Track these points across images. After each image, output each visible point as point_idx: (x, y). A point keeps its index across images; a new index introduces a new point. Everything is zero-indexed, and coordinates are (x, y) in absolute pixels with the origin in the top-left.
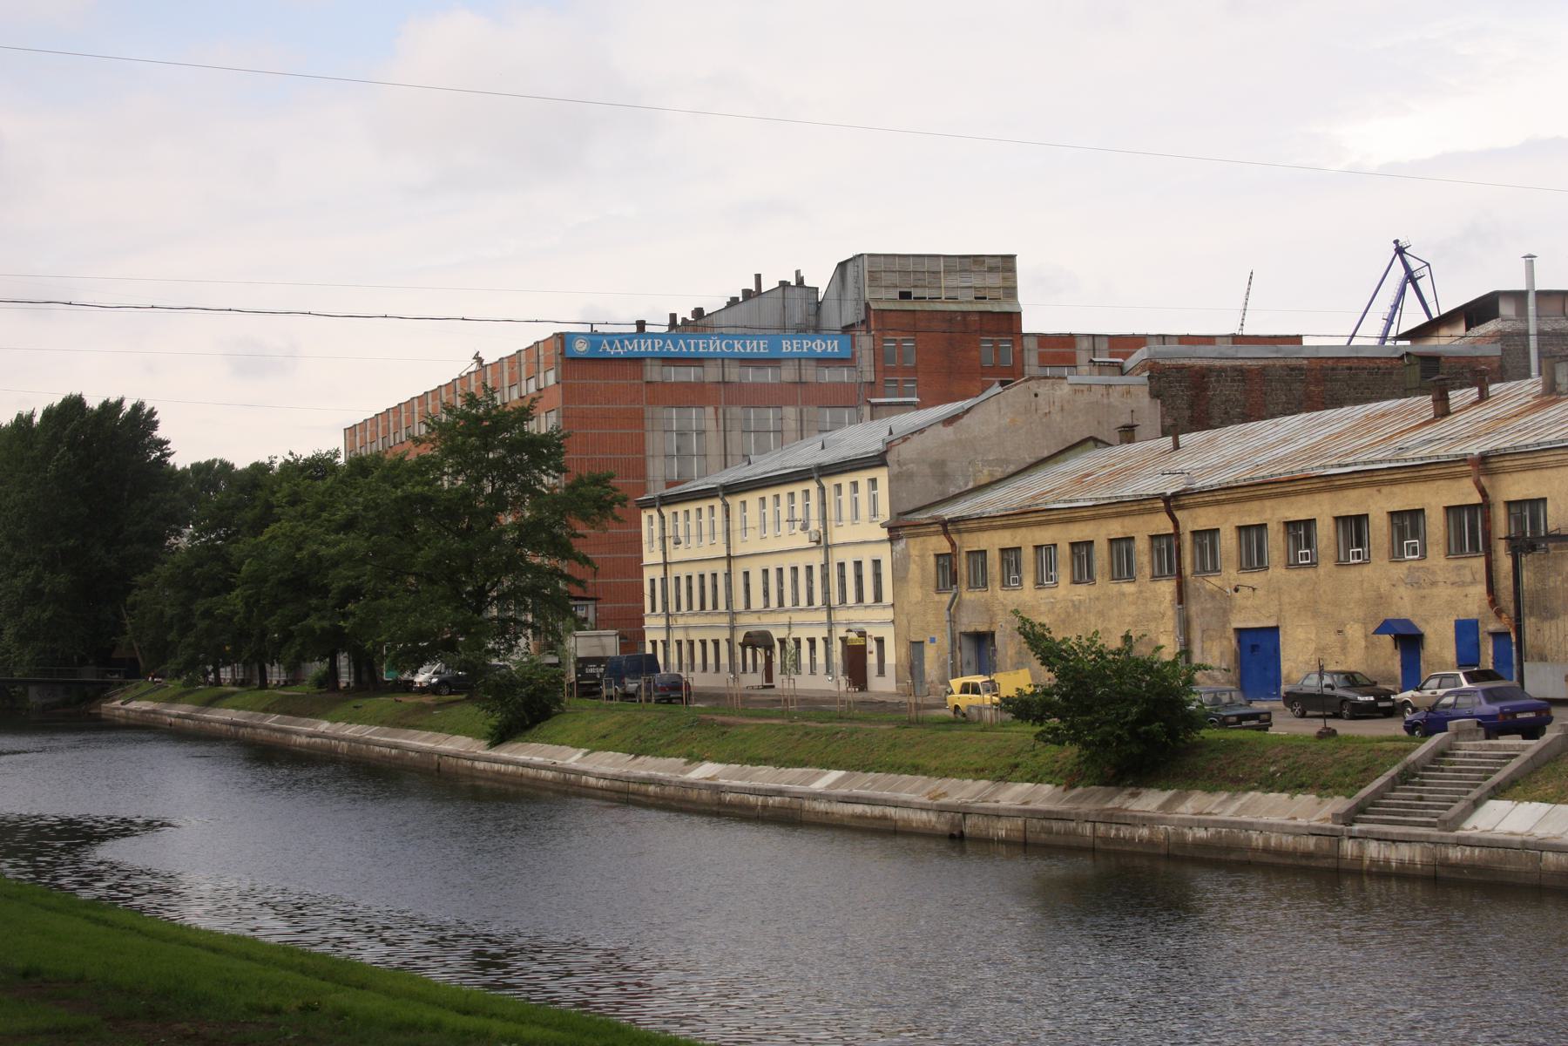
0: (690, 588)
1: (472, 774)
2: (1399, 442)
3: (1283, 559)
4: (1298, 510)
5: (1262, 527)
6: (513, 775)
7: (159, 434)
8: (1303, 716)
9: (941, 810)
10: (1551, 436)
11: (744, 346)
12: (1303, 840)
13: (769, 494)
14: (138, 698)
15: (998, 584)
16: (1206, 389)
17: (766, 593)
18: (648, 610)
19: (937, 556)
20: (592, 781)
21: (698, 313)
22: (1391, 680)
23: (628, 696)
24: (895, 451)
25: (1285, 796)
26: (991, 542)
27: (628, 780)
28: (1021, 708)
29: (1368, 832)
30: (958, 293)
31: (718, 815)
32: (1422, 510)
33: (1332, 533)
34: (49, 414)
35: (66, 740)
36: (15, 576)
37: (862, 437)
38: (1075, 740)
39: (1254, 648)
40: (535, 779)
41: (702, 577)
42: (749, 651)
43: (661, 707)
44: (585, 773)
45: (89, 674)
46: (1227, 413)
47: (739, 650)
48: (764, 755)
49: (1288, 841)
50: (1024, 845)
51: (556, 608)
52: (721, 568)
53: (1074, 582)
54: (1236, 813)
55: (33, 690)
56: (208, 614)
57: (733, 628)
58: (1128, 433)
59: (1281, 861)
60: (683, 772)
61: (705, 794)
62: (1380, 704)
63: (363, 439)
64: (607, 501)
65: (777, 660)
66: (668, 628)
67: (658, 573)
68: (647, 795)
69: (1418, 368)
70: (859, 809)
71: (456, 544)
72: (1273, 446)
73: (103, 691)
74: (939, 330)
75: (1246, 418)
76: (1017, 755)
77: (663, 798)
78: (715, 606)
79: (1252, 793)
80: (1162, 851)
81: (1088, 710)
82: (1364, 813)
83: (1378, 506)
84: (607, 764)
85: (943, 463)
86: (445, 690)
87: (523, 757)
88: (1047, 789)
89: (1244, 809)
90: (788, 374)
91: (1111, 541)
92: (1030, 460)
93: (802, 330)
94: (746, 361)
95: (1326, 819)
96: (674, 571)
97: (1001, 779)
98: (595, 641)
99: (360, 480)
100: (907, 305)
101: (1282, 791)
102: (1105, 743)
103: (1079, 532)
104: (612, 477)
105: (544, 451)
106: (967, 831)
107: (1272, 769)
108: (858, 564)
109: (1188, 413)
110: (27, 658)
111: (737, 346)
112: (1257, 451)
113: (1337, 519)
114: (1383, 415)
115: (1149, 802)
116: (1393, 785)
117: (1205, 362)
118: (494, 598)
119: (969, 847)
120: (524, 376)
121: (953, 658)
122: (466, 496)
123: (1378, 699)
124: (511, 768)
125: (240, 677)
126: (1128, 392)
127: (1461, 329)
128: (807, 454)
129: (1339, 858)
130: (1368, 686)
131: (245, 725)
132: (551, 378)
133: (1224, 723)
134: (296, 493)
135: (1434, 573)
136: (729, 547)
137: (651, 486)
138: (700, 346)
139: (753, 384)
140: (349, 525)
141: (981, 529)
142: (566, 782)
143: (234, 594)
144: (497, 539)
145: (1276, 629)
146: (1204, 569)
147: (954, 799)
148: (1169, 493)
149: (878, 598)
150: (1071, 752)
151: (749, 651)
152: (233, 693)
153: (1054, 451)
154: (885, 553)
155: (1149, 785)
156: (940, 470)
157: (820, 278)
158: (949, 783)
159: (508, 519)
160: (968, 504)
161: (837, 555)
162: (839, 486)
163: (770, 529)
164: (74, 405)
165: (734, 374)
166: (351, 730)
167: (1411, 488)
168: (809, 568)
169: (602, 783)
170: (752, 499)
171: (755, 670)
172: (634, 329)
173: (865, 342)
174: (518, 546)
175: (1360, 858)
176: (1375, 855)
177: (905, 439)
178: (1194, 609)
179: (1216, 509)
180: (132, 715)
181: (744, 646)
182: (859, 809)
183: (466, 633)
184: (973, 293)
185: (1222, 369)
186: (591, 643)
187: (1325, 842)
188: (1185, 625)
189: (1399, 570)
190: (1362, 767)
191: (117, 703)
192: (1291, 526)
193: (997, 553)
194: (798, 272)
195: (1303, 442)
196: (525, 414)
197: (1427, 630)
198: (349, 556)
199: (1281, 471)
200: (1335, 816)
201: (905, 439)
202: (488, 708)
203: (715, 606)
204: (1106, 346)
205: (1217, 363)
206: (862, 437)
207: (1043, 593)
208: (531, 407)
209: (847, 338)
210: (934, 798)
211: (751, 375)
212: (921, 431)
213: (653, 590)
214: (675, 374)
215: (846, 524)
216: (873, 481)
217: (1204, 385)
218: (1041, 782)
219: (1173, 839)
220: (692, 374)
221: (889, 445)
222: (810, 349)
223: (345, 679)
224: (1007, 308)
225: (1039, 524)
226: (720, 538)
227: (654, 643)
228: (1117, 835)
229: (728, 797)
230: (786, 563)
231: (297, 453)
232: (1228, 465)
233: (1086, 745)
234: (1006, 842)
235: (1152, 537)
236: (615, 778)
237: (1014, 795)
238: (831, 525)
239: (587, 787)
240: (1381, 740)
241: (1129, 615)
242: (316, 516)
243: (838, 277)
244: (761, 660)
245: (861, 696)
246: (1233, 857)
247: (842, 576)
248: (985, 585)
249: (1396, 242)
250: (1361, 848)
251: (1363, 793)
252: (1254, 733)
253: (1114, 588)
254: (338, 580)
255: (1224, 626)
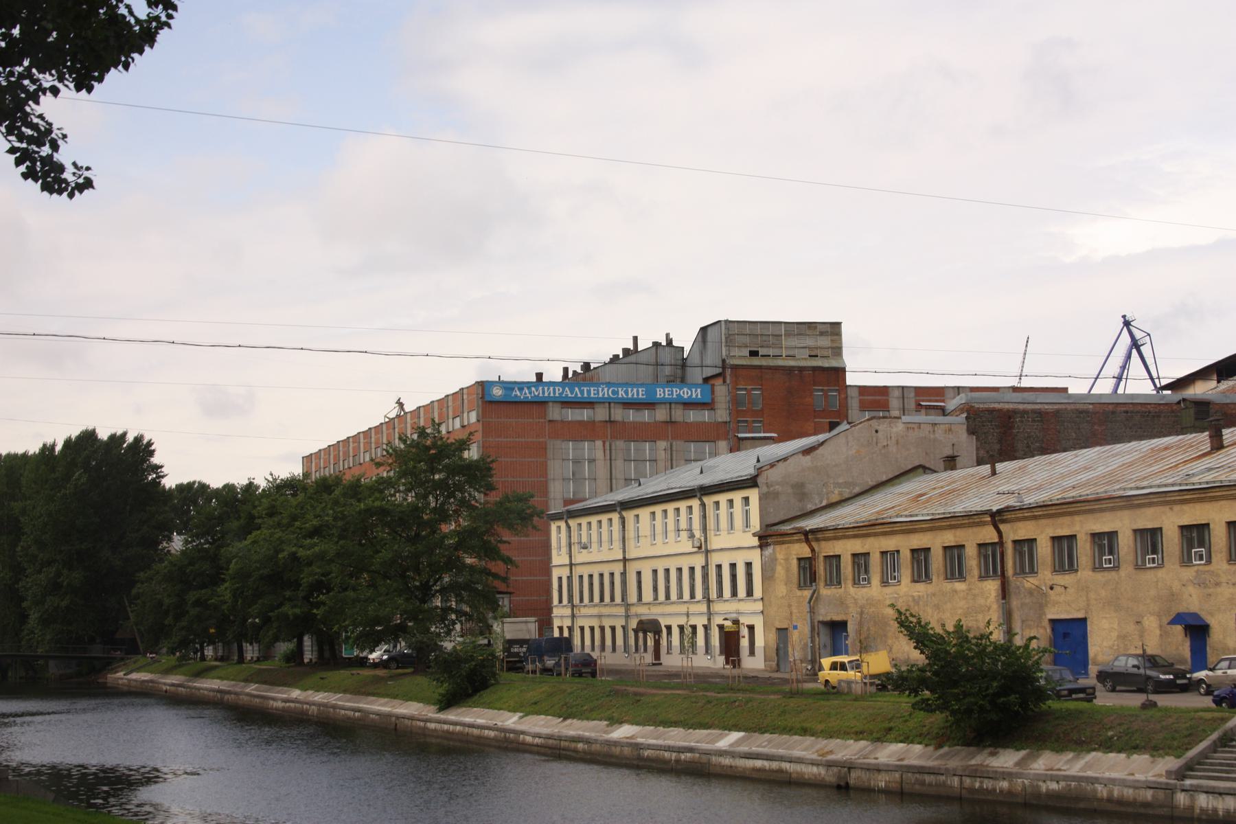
0: (591, 584)
1: (425, 732)
2: (1185, 469)
3: (1090, 564)
4: (1102, 524)
5: (1072, 538)
6: (460, 733)
7: (155, 460)
8: (1113, 690)
9: (829, 765)
10: (1224, 477)
11: (626, 393)
12: (1142, 792)
13: (658, 509)
14: (138, 670)
15: (850, 583)
16: (1012, 428)
17: (655, 589)
18: (556, 601)
19: (799, 559)
20: (529, 739)
21: (586, 366)
22: (1183, 662)
23: (546, 671)
24: (764, 475)
25: (1123, 756)
26: (846, 548)
27: (560, 739)
28: (884, 683)
29: (1198, 786)
30: (819, 353)
31: (638, 767)
32: (1208, 525)
33: (1131, 543)
34: (68, 443)
35: (82, 704)
36: (40, 572)
37: (738, 464)
38: (941, 708)
39: (1066, 635)
40: (479, 737)
41: (601, 575)
42: (641, 635)
43: (577, 680)
44: (523, 733)
45: (97, 651)
46: (1028, 447)
47: (632, 634)
48: (674, 719)
49: (1129, 793)
50: (900, 795)
51: (483, 598)
52: (618, 569)
53: (914, 581)
54: (1081, 770)
55: (51, 663)
56: (198, 603)
57: (627, 617)
58: (951, 462)
59: (1123, 809)
60: (606, 732)
61: (627, 751)
62: (1179, 682)
63: (318, 465)
64: (527, 515)
65: (664, 642)
66: (573, 616)
67: (565, 573)
68: (576, 751)
69: (1192, 411)
70: (759, 763)
71: (407, 550)
72: (1077, 472)
73: (108, 664)
74: (776, 382)
75: (1044, 451)
76: (890, 720)
77: (591, 753)
78: (612, 599)
79: (1094, 754)
80: (1020, 800)
81: (955, 684)
82: (1192, 770)
83: (1171, 521)
84: (540, 726)
85: (802, 485)
86: (394, 665)
87: (468, 720)
88: (918, 748)
89: (1088, 766)
90: (661, 414)
91: (945, 548)
92: (872, 483)
93: (670, 381)
94: (628, 404)
95: (1160, 776)
96: (578, 571)
97: (878, 740)
98: (523, 626)
99: (325, 496)
100: (756, 361)
101: (1120, 752)
102: (969, 711)
103: (918, 541)
104: (532, 496)
105: (478, 473)
106: (852, 782)
107: (1110, 733)
108: (733, 566)
109: (997, 447)
110: (48, 637)
111: (621, 393)
112: (1063, 476)
113: (1135, 531)
114: (1166, 449)
115: (1007, 760)
116: (1214, 748)
117: (1011, 406)
118: (437, 591)
119: (852, 793)
120: (451, 416)
121: (813, 641)
122: (415, 509)
123: (1176, 677)
124: (458, 728)
125: (220, 653)
126: (950, 430)
127: (1213, 383)
128: (688, 477)
129: (1173, 807)
130: (1167, 667)
131: (229, 692)
132: (473, 417)
133: (1059, 696)
134: (274, 507)
135: (1218, 575)
136: (624, 552)
137: (552, 503)
138: (592, 393)
139: (634, 422)
140: (316, 532)
141: (836, 538)
142: (506, 739)
143: (223, 587)
144: (440, 543)
145: (1084, 620)
146: (1023, 571)
147: (839, 756)
148: (995, 509)
149: (750, 592)
150: (939, 718)
151: (641, 635)
152: (216, 667)
153: (891, 476)
154: (755, 557)
155: (1005, 746)
156: (800, 491)
157: (685, 339)
158: (834, 743)
159: (448, 528)
160: (823, 518)
161: (715, 559)
162: (717, 503)
163: (659, 538)
164: (88, 437)
165: (618, 414)
166: (319, 697)
167: (1198, 506)
168: (692, 569)
169: (537, 741)
170: (644, 513)
171: (645, 650)
172: (534, 379)
173: (721, 391)
174: (456, 549)
175: (1192, 808)
176: (1204, 805)
177: (772, 465)
178: (1015, 603)
179: (1033, 522)
180: (133, 684)
181: (636, 631)
182: (759, 763)
183: (415, 619)
184: (807, 352)
185: (1025, 412)
186: (514, 629)
187: (1161, 794)
188: (1008, 616)
189: (1188, 573)
190: (1186, 733)
191: (121, 674)
192: (1096, 536)
193: (849, 558)
194: (667, 335)
195: (1101, 470)
196: (463, 445)
197: (1212, 622)
198: (321, 556)
199: (1087, 492)
200: (1169, 773)
201: (772, 465)
202: (438, 680)
203: (612, 599)
204: (912, 394)
205: (1021, 407)
206: (738, 464)
207: (889, 590)
208: (469, 439)
209: (708, 387)
210: (822, 755)
211: (632, 416)
212: (785, 459)
213: (560, 586)
214: (571, 415)
215: (723, 533)
216: (746, 500)
217: (1010, 425)
218: (912, 742)
219: (1029, 790)
220: (585, 415)
221: (760, 470)
222: (679, 395)
223: (308, 656)
224: (833, 363)
225: (885, 534)
226: (617, 544)
227: (561, 629)
228: (981, 787)
229: (646, 753)
230: (673, 565)
231: (276, 474)
232: (1039, 488)
233: (953, 713)
234: (886, 792)
235: (980, 545)
236: (549, 737)
237: (889, 753)
238: (711, 534)
239: (524, 743)
240: (1197, 711)
241: (967, 606)
242: (289, 525)
243: (700, 339)
244: (650, 643)
245: (736, 672)
246: (1082, 805)
247: (719, 576)
248: (839, 583)
249: (1124, 317)
250: (1192, 799)
251: (1191, 753)
252: (1085, 704)
253: (948, 586)
254: (307, 577)
255: (1040, 618)
